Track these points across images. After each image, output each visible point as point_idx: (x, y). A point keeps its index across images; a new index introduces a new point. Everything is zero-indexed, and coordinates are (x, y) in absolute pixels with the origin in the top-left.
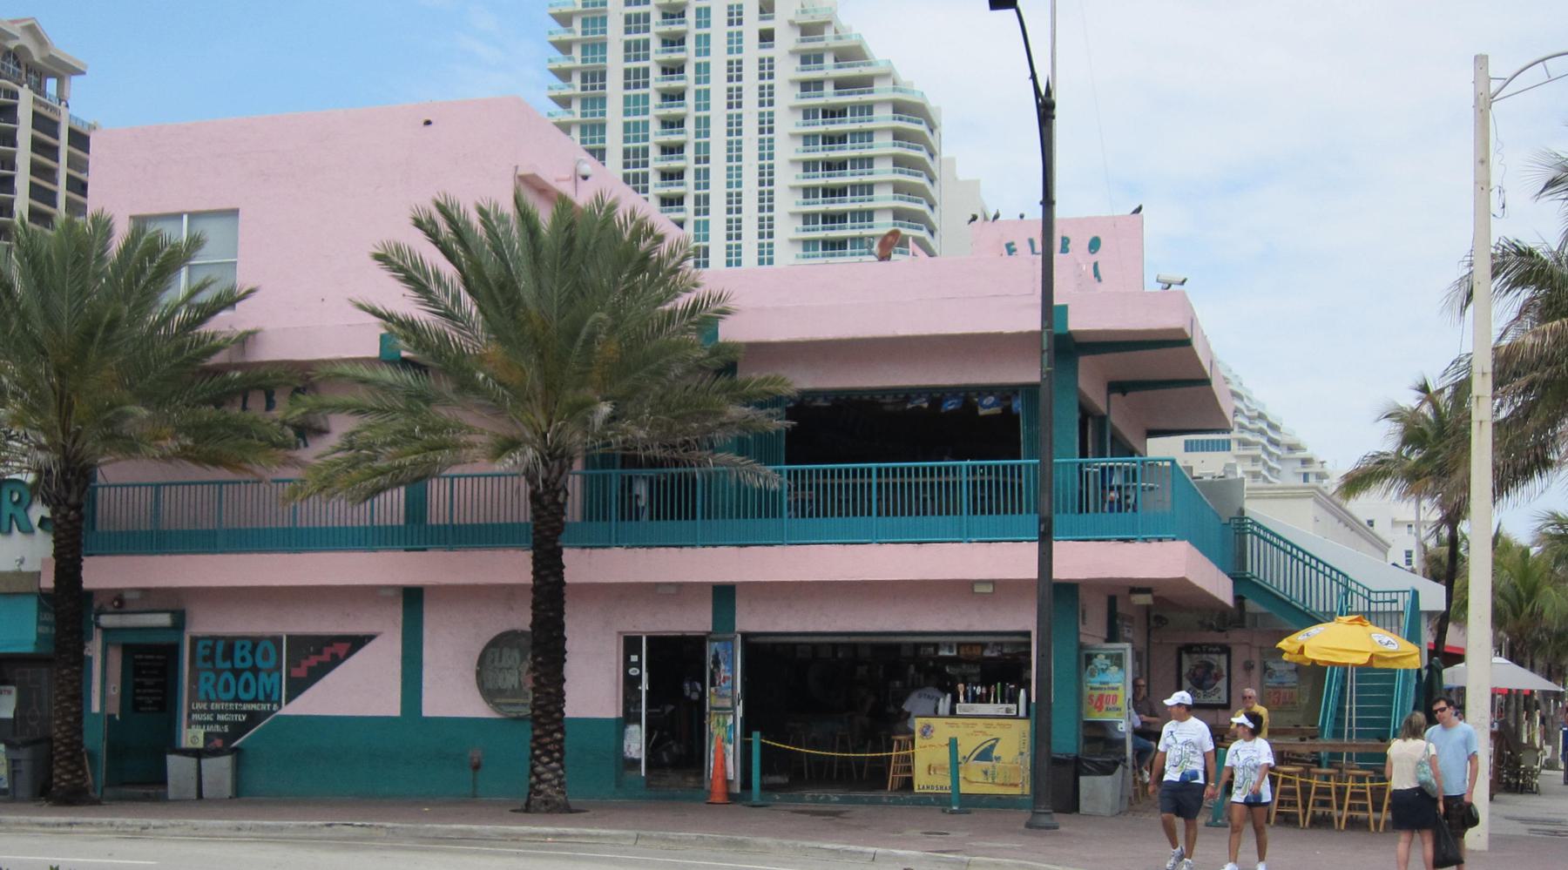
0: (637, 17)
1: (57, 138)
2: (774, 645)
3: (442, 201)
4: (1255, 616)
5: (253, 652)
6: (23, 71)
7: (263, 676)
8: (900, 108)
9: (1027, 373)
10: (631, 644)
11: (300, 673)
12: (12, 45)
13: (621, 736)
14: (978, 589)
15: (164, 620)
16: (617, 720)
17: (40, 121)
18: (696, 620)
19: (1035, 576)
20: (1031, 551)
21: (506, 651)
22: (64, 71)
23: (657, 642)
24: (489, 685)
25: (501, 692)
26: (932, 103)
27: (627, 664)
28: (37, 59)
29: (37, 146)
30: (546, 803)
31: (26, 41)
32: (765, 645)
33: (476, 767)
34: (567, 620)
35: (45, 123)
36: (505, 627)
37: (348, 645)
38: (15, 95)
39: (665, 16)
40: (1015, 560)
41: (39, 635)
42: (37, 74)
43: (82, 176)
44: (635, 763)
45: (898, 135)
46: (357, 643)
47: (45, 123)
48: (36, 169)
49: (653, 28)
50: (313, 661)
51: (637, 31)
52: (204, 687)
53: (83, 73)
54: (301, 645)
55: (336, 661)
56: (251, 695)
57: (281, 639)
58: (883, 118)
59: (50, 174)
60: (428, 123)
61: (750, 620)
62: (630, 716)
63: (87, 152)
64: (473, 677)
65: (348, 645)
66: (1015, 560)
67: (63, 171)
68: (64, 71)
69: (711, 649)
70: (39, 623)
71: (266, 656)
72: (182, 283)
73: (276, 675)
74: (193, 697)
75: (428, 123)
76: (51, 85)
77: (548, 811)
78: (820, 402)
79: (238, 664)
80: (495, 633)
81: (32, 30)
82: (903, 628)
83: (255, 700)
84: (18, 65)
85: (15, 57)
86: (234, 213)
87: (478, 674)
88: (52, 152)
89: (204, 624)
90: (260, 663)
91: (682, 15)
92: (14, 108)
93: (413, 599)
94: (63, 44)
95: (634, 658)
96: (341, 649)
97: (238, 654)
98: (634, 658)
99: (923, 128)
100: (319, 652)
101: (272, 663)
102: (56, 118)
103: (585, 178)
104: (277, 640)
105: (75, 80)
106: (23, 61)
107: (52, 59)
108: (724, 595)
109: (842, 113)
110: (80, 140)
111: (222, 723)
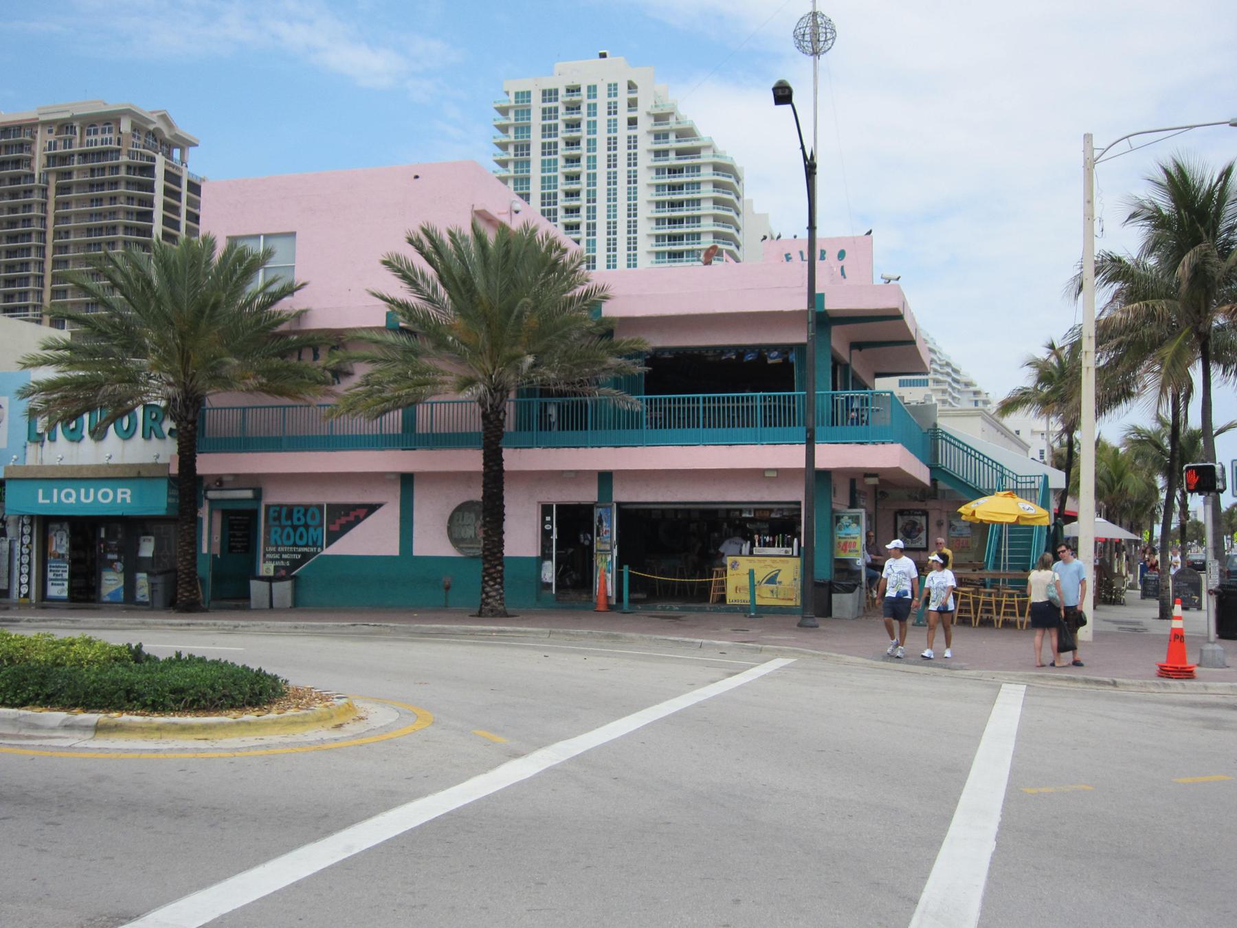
2: (637, 510)
4: (944, 491)
5: (305, 515)
7: (311, 530)
8: (717, 168)
9: (799, 336)
10: (546, 509)
11: (335, 528)
12: (151, 127)
14: (767, 474)
15: (248, 494)
16: (537, 558)
18: (588, 494)
20: (801, 450)
21: (466, 514)
22: (185, 144)
23: (562, 508)
24: (456, 536)
25: (463, 540)
26: (738, 164)
27: (544, 522)
28: (167, 136)
29: (167, 192)
33: (448, 588)
36: (466, 499)
37: (365, 510)
38: (153, 159)
39: (568, 109)
40: (791, 456)
42: (167, 146)
44: (549, 585)
45: (717, 185)
46: (372, 508)
48: (167, 206)
50: (343, 520)
52: (274, 537)
54: (335, 509)
55: (358, 520)
56: (304, 542)
58: (707, 174)
60: (417, 177)
61: (622, 494)
62: (545, 556)
64: (445, 531)
65: (365, 510)
68: (185, 144)
69: (597, 512)
70: (169, 496)
71: (313, 517)
72: (260, 279)
73: (319, 529)
74: (267, 544)
75: (417, 177)
76: (176, 153)
78: (666, 355)
79: (296, 523)
81: (164, 118)
82: (720, 499)
83: (307, 545)
86: (293, 234)
87: (449, 529)
88: (177, 196)
89: (274, 497)
90: (310, 522)
91: (579, 108)
92: (153, 167)
93: (407, 481)
94: (184, 126)
95: (548, 519)
96: (362, 512)
97: (295, 516)
98: (548, 519)
99: (732, 180)
100: (347, 515)
101: (316, 522)
102: (178, 173)
103: (517, 212)
104: (320, 507)
105: (192, 150)
106: (158, 138)
107: (177, 136)
108: (605, 479)
109: (681, 171)
110: (195, 188)
111: (285, 560)
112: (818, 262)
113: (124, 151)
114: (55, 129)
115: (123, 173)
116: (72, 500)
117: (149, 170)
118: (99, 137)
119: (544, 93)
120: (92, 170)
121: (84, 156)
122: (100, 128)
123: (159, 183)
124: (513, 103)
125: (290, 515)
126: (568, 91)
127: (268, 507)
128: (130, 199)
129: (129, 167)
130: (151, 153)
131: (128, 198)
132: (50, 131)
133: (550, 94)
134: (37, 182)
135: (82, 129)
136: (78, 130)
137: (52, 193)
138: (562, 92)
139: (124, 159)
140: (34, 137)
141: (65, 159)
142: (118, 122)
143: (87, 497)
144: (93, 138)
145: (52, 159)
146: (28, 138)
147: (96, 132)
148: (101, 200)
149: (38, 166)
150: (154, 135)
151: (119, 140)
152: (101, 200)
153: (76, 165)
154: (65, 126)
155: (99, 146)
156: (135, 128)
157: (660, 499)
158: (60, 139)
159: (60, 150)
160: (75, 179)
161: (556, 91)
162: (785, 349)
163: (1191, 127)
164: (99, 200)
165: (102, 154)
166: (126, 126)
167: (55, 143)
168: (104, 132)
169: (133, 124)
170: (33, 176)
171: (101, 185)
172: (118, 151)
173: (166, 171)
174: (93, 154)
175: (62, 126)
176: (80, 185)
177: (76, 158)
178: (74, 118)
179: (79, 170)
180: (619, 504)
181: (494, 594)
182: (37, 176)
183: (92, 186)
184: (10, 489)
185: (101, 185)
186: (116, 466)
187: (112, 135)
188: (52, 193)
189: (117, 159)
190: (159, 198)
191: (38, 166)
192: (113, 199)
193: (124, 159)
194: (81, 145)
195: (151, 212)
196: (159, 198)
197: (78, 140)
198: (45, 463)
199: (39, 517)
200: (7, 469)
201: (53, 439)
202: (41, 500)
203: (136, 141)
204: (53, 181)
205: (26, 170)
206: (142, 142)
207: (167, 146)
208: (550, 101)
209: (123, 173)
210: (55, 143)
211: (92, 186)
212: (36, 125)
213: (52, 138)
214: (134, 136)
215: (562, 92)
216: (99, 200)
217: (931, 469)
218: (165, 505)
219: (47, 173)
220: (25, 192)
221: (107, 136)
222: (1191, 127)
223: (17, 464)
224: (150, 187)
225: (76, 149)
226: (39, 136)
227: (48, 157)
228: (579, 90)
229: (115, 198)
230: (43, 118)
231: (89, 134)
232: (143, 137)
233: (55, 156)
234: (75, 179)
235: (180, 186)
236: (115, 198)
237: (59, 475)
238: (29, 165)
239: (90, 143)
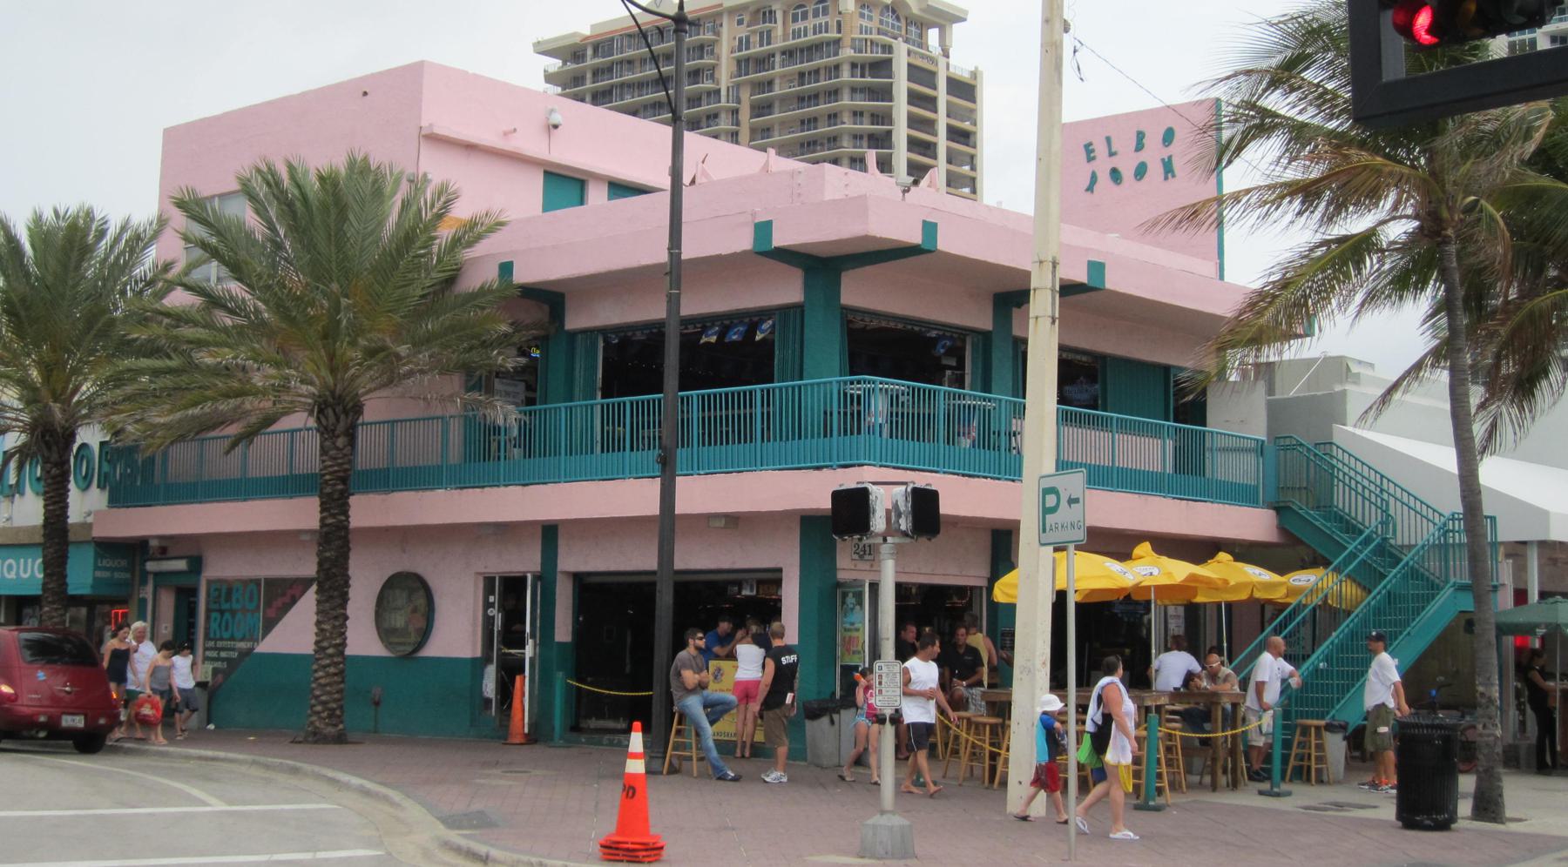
1: (935, 88)
3: (295, 164)
6: (903, 24)
10: (489, 582)
13: (478, 676)
15: (181, 565)
16: (474, 660)
17: (915, 73)
18: (526, 561)
19: (657, 512)
20: (653, 488)
22: (947, 20)
24: (386, 625)
28: (915, 11)
29: (914, 98)
30: (315, 734)
32: (696, 583)
33: (377, 704)
34: (352, 563)
38: (888, 48)
40: (635, 496)
41: (95, 579)
47: (919, 74)
48: (914, 121)
53: (964, 20)
57: (523, 580)
59: (928, 125)
60: (365, 94)
61: (573, 560)
63: (974, 101)
67: (942, 122)
68: (947, 20)
70: (96, 568)
74: (207, 637)
75: (365, 94)
76: (933, 35)
77: (316, 742)
78: (639, 336)
80: (391, 573)
82: (713, 566)
84: (898, 19)
85: (894, 11)
87: (377, 613)
88: (930, 103)
89: (218, 568)
92: (889, 62)
95: (491, 599)
101: (252, 606)
103: (556, 127)
104: (257, 582)
108: (550, 533)
110: (964, 89)
112: (687, 192)
113: (847, 41)
114: (746, 18)
115: (846, 76)
116: (12, 575)
117: (882, 67)
118: (811, 23)
120: (801, 75)
121: (789, 53)
122: (810, 8)
123: (901, 85)
127: (209, 582)
128: (857, 114)
129: (854, 66)
130: (888, 39)
131: (855, 114)
132: (740, 22)
134: (723, 103)
136: (779, 16)
137: (745, 115)
139: (847, 53)
140: (718, 34)
141: (763, 62)
144: (800, 25)
145: (743, 65)
146: (709, 36)
147: (805, 16)
148: (815, 119)
149: (725, 77)
152: (815, 119)
153: (778, 70)
155: (811, 37)
158: (754, 32)
159: (756, 49)
160: (778, 90)
164: (812, 121)
167: (748, 38)
168: (816, 15)
170: (718, 92)
171: (814, 98)
172: (837, 42)
173: (909, 65)
174: (802, 51)
176: (784, 99)
177: (778, 58)
179: (783, 76)
181: (319, 708)
182: (723, 93)
183: (802, 100)
185: (814, 98)
187: (827, 19)
188: (745, 115)
189: (836, 54)
190: (901, 108)
191: (725, 77)
192: (833, 117)
193: (847, 53)
195: (889, 133)
196: (901, 108)
201: (22, 494)
203: (865, 23)
204: (746, 96)
205: (708, 85)
206: (874, 24)
209: (846, 76)
210: (748, 38)
211: (802, 100)
212: (720, 14)
213: (742, 32)
214: (862, 16)
216: (812, 121)
218: (90, 581)
219: (738, 86)
220: (708, 117)
221: (822, 20)
224: (886, 93)
225: (778, 43)
226: (725, 30)
227: (739, 62)
229: (835, 115)
231: (795, 20)
232: (876, 16)
233: (747, 60)
234: (778, 90)
236: (835, 115)
238: (712, 76)
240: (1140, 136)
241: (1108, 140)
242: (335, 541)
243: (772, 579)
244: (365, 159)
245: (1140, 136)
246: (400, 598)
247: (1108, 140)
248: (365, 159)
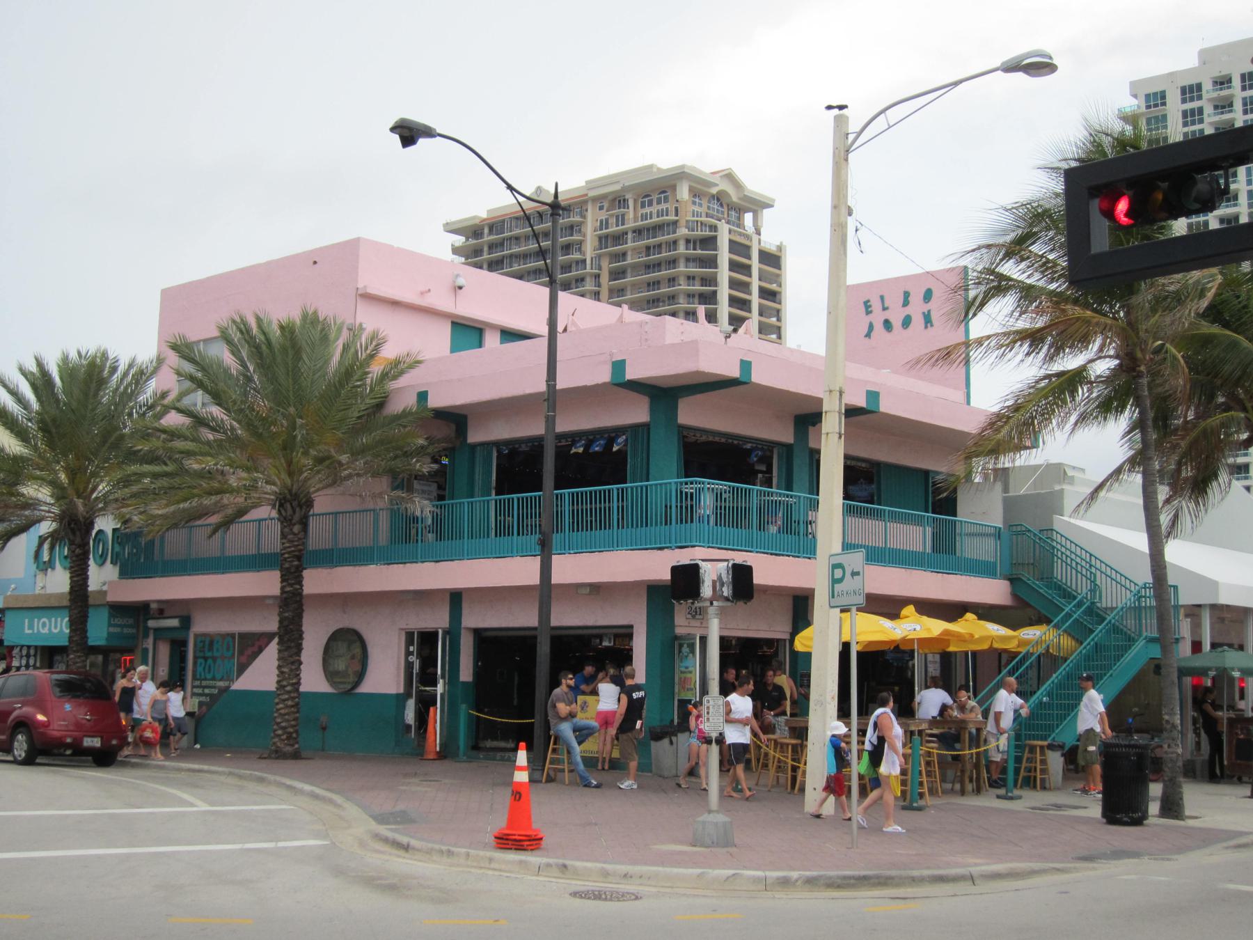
0: (1192, 111)
2: (509, 637)
10: (410, 636)
12: (714, 191)
15: (174, 623)
16: (398, 695)
17: (735, 247)
18: (437, 620)
20: (534, 564)
22: (758, 205)
24: (331, 669)
28: (735, 199)
29: (734, 266)
30: (276, 752)
31: (724, 186)
33: (324, 729)
35: (740, 248)
38: (714, 228)
39: (1216, 107)
40: (521, 570)
42: (738, 210)
43: (774, 287)
44: (409, 727)
47: (740, 248)
48: (734, 284)
49: (1207, 119)
51: (1193, 123)
52: (200, 669)
54: (244, 637)
56: (209, 676)
57: (436, 633)
59: (745, 287)
61: (474, 618)
62: (408, 694)
66: (521, 570)
68: (758, 205)
70: (110, 625)
72: (1042, 355)
74: (194, 678)
76: (748, 218)
77: (277, 758)
78: (524, 448)
79: (216, 654)
81: (730, 177)
84: (721, 205)
85: (718, 200)
88: (746, 269)
89: (204, 625)
91: (1231, 105)
92: (715, 238)
94: (755, 184)
95: (411, 649)
97: (215, 646)
101: (230, 653)
102: (747, 243)
103: (460, 288)
104: (232, 636)
105: (766, 211)
106: (724, 201)
107: (747, 199)
108: (456, 598)
110: (772, 259)
111: (206, 695)
113: (683, 222)
114: (606, 205)
115: (682, 249)
116: (46, 631)
117: (710, 242)
118: (655, 208)
119: (1183, 90)
120: (648, 248)
121: (638, 232)
122: (655, 197)
123: (724, 256)
124: (1143, 109)
125: (211, 643)
126: (1215, 83)
127: (196, 636)
128: (691, 278)
129: (688, 241)
131: (689, 278)
132: (601, 208)
133: (1191, 90)
134: (588, 270)
135: (635, 201)
136: (631, 203)
137: (605, 279)
138: (1207, 86)
139: (683, 231)
140: (584, 217)
141: (619, 238)
142: (674, 188)
143: (31, 627)
144: (647, 210)
145: (603, 240)
148: (659, 282)
149: (590, 249)
150: (719, 198)
151: (676, 209)
152: (659, 282)
153: (630, 244)
154: (618, 200)
155: (655, 219)
156: (695, 194)
157: (504, 625)
158: (612, 215)
159: (613, 229)
161: (1199, 87)
162: (610, 434)
163: (956, 84)
164: (655, 284)
165: (657, 229)
166: (684, 193)
167: (607, 220)
168: (659, 202)
169: (691, 190)
170: (584, 261)
171: (657, 266)
172: (675, 223)
173: (731, 241)
174: (648, 230)
175: (614, 200)
176: (635, 267)
177: (630, 236)
178: (625, 189)
179: (634, 249)
180: (478, 633)
181: (280, 732)
182: (588, 262)
183: (648, 267)
184: (9, 619)
185: (657, 266)
186: (51, 595)
187: (668, 205)
188: (605, 279)
189: (674, 232)
190: (724, 274)
191: (590, 249)
192: (672, 280)
193: (683, 231)
194: (635, 220)
196: (724, 274)
197: (631, 215)
198: (49, 591)
199: (44, 648)
200: (6, 598)
201: (53, 568)
202: (27, 631)
203: (696, 208)
204: (606, 265)
205: (577, 256)
206: (703, 210)
207: (738, 210)
208: (1192, 99)
209: (682, 249)
210: (607, 220)
211: (648, 267)
212: (585, 202)
213: (603, 215)
214: (694, 203)
215: (1207, 86)
216: (655, 284)
217: (1010, 580)
218: (105, 635)
219: (599, 257)
220: (577, 281)
221: (663, 206)
222: (956, 84)
223: (16, 593)
224: (712, 262)
225: (630, 224)
226: (589, 215)
227: (600, 238)
228: (1230, 81)
229: (674, 279)
230: (592, 194)
231: (643, 206)
232: (705, 202)
233: (607, 237)
235: (749, 258)
236: (674, 279)
237: (37, 605)
238: (580, 249)
239: (644, 217)
240: (907, 295)
241: (882, 298)
242: (292, 604)
243: (626, 634)
244: (315, 312)
245: (907, 295)
246: (341, 648)
247: (882, 298)
248: (315, 312)
